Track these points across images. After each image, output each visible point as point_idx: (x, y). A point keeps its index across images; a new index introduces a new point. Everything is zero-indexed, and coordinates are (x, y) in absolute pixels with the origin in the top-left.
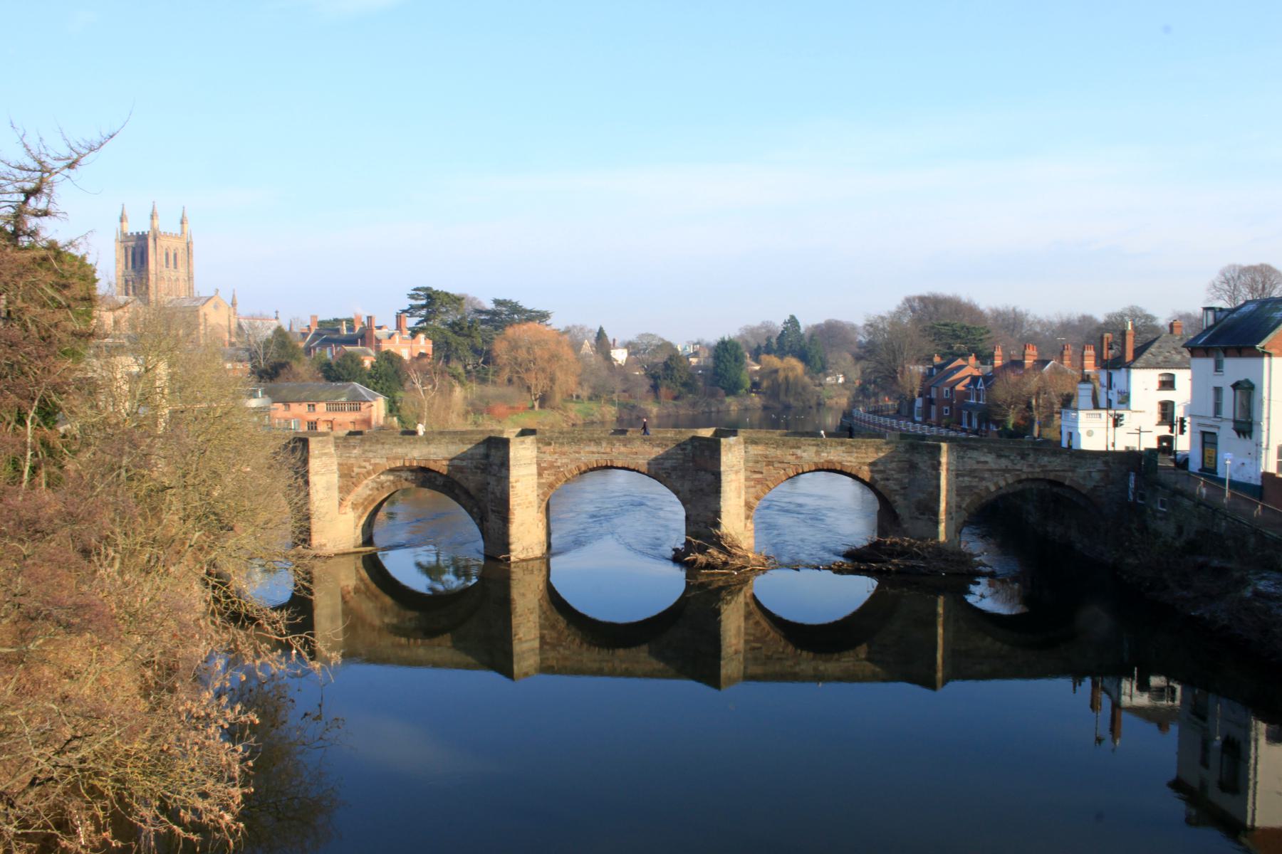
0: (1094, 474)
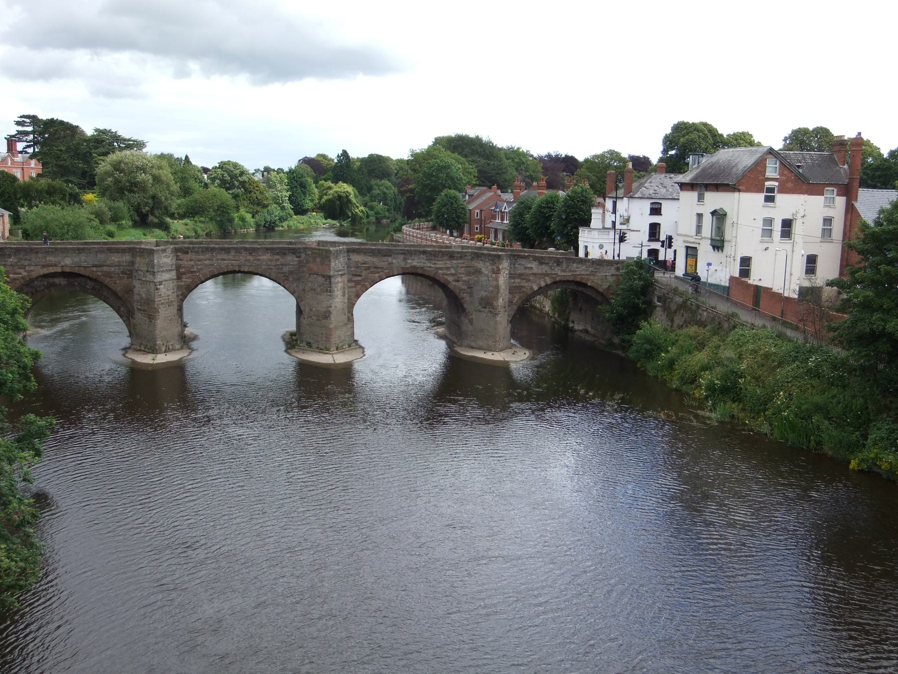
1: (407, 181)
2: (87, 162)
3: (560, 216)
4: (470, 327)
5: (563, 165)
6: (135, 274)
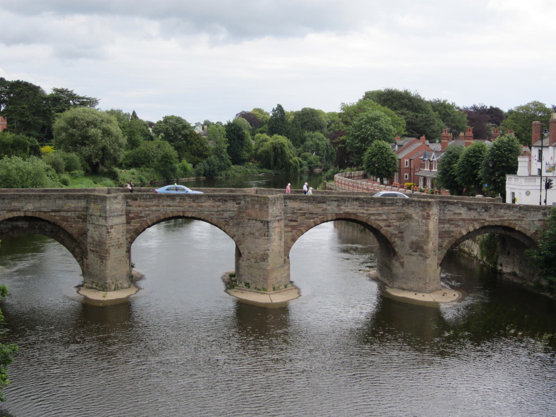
0: (536, 223)
1: (340, 133)
2: (48, 119)
3: (487, 165)
4: (401, 270)
5: (488, 117)
6: (89, 218)
